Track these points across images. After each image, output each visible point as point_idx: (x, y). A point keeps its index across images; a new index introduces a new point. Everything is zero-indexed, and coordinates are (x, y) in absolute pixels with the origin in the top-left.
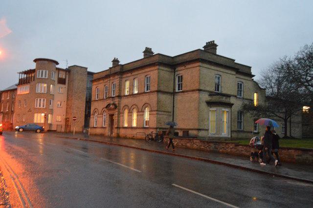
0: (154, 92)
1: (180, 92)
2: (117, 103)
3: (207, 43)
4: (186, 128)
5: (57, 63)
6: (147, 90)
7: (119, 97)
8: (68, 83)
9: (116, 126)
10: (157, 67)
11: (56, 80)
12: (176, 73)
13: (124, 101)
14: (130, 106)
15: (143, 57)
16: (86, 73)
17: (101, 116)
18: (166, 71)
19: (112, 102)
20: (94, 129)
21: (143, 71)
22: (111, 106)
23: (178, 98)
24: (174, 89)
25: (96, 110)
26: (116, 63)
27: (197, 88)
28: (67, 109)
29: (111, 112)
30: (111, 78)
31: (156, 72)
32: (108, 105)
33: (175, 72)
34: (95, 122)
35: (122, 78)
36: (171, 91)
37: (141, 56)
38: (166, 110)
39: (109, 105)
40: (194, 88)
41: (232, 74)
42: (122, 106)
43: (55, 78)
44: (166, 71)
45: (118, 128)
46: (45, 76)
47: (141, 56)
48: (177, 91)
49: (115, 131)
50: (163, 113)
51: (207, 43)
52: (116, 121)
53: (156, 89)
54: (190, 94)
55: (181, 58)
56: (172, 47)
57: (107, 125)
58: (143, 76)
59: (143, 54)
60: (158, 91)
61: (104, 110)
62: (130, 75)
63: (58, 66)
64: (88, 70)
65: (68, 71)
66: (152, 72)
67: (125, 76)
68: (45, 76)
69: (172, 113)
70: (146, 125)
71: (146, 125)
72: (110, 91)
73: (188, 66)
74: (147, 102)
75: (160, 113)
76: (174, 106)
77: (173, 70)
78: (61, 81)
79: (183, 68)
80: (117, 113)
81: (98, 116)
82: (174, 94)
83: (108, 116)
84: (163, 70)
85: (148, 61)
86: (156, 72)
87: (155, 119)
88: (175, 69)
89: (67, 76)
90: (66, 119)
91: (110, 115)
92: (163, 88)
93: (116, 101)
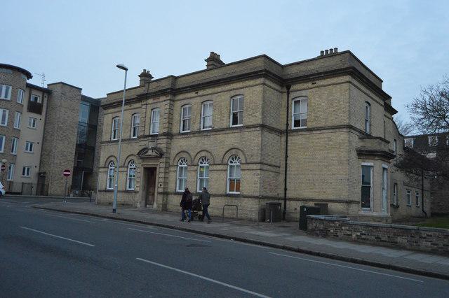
0: (254, 126)
1: (301, 130)
2: (163, 146)
3: (322, 52)
4: (321, 197)
5: (29, 76)
6: (114, 138)
7: (169, 135)
8: (47, 111)
9: (161, 190)
10: (261, 80)
11: (25, 103)
12: (292, 95)
13: (179, 144)
14: (193, 154)
15: (138, 84)
16: (79, 98)
17: (125, 169)
18: (274, 89)
19: (151, 145)
20: (108, 194)
21: (227, 87)
22: (150, 153)
23: (296, 140)
24: (287, 125)
25: (112, 159)
26: (147, 79)
27: (346, 122)
28: (41, 156)
29: (150, 164)
30: (150, 101)
31: (260, 89)
32: (144, 149)
33: (288, 93)
34: (108, 181)
35: (174, 101)
36: (284, 128)
37: (204, 66)
38: (273, 164)
39: (145, 150)
40: (337, 123)
41: (379, 104)
42: (174, 152)
43: (23, 99)
44: (274, 89)
45: (166, 194)
46: (6, 96)
47: (204, 66)
48: (293, 128)
49: (159, 199)
50: (269, 167)
51: (322, 52)
52: (161, 180)
53: (260, 122)
54: (327, 134)
55: (302, 68)
56: (289, 51)
57: (138, 185)
58: (226, 96)
59: (139, 78)
60: (263, 126)
61: (130, 158)
62: (193, 94)
63: (30, 81)
64: (84, 93)
65: (47, 92)
66: (247, 89)
67: (181, 97)
68: (6, 96)
69: (283, 169)
70: (110, 187)
71: (110, 187)
72: (147, 124)
73: (319, 83)
74: (236, 145)
75: (265, 167)
76: (287, 156)
77: (285, 90)
78: (34, 108)
79: (310, 85)
80: (163, 165)
81: (211, 168)
82: (287, 132)
83: (141, 170)
84: (270, 87)
85: (217, 74)
86: (260, 89)
87: (257, 178)
88: (288, 88)
89: (45, 100)
90: (39, 174)
91: (146, 169)
92: (270, 121)
93: (162, 143)
